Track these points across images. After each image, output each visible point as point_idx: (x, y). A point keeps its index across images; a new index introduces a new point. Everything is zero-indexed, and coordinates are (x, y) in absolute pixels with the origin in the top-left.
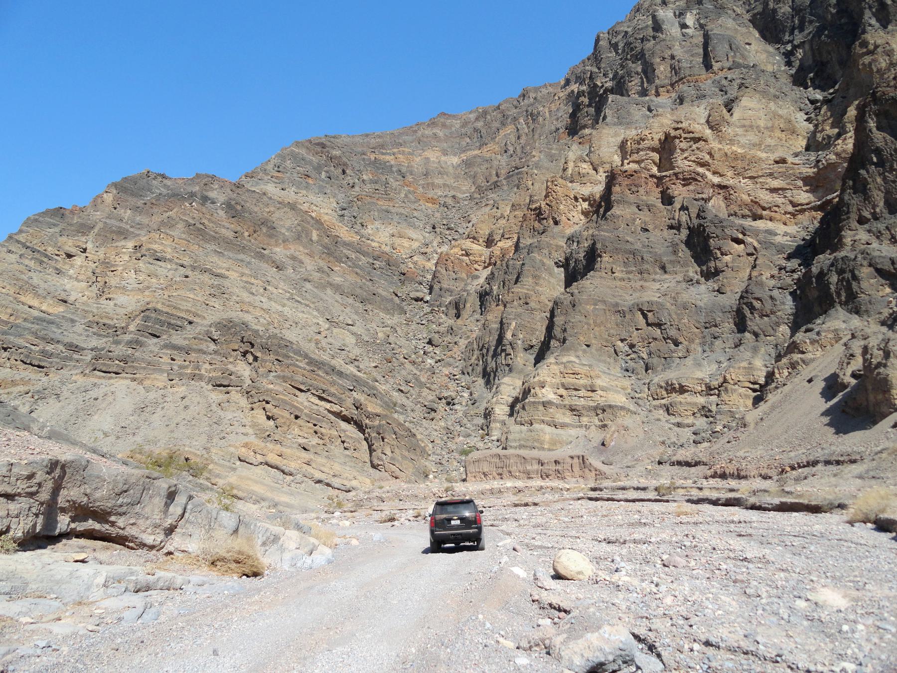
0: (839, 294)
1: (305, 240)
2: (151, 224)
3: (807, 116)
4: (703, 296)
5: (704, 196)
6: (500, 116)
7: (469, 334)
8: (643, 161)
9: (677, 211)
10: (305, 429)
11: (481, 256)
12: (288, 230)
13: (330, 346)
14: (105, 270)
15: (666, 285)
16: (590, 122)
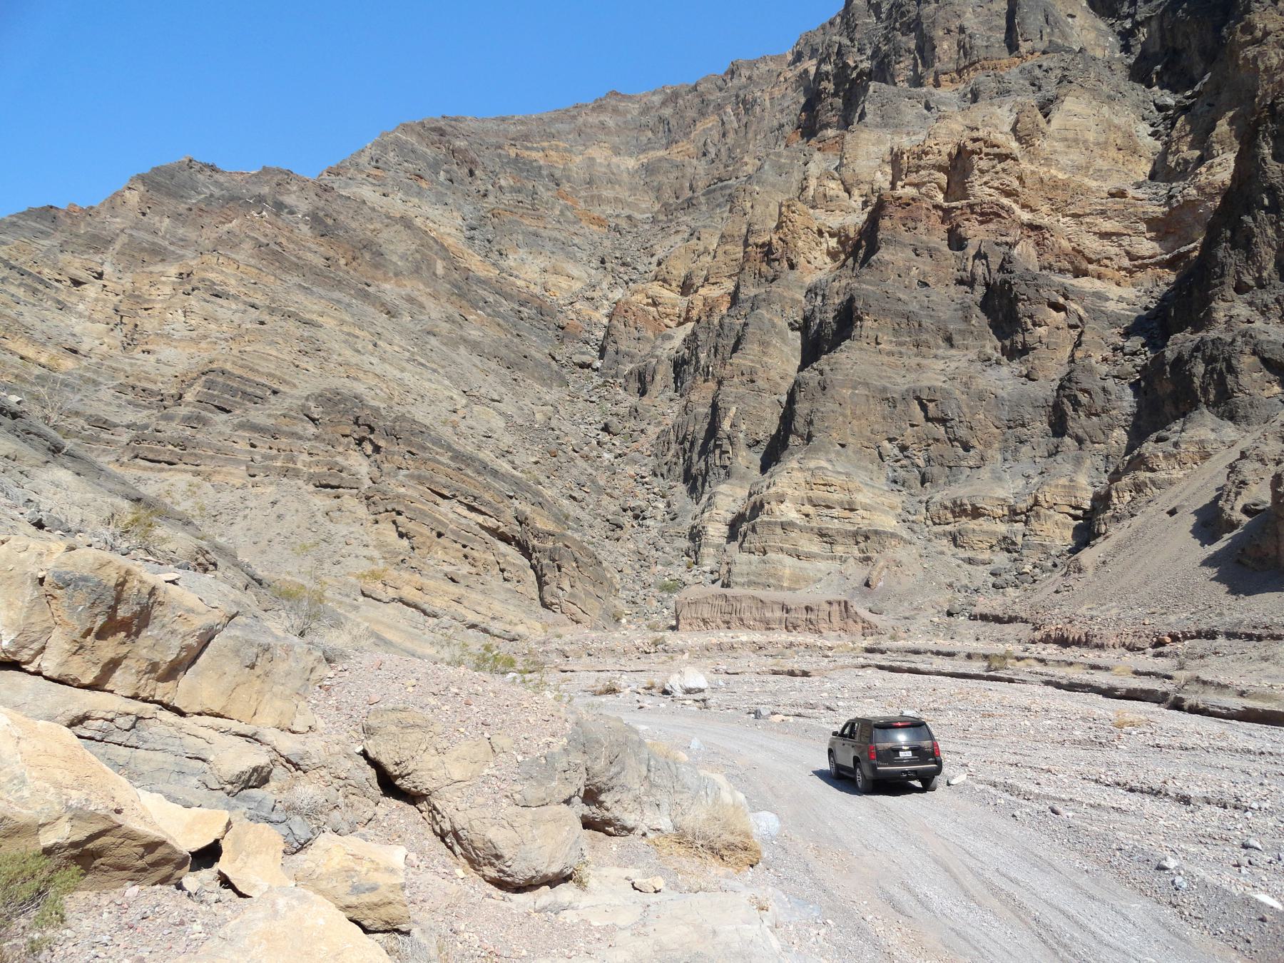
0: (1205, 391)
1: (425, 274)
2: (200, 240)
3: (1152, 129)
4: (1006, 382)
5: (1008, 239)
6: (697, 100)
7: (660, 418)
8: (924, 184)
9: (971, 259)
10: (451, 551)
11: (674, 307)
12: (401, 257)
13: (472, 431)
14: (134, 307)
15: (953, 365)
16: (835, 119)
